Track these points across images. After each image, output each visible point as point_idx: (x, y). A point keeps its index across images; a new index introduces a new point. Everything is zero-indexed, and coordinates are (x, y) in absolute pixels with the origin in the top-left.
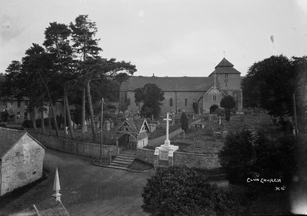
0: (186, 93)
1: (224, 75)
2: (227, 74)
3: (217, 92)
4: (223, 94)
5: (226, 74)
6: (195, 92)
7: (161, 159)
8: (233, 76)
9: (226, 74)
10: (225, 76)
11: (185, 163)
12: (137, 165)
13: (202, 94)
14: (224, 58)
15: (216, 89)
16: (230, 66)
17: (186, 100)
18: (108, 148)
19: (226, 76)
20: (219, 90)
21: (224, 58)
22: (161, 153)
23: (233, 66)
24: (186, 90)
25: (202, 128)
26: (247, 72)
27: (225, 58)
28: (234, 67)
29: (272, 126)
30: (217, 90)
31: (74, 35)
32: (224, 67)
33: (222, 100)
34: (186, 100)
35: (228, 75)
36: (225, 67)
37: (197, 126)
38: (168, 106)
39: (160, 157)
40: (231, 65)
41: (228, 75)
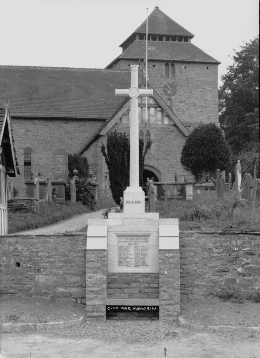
2: (173, 63)
3: (152, 119)
5: (170, 64)
8: (196, 71)
9: (167, 63)
12: (207, 188)
13: (100, 124)
14: (157, 8)
15: (149, 108)
16: (180, 38)
17: (132, 255)
18: (250, 230)
19: (167, 73)
20: (162, 111)
21: (157, 8)
26: (225, 75)
27: (160, 9)
28: (193, 41)
29: (200, 284)
30: (152, 110)
31: (185, 317)
33: (185, 149)
34: (132, 255)
35: (177, 66)
36: (161, 43)
38: (76, 202)
39: (114, 257)
40: (182, 34)
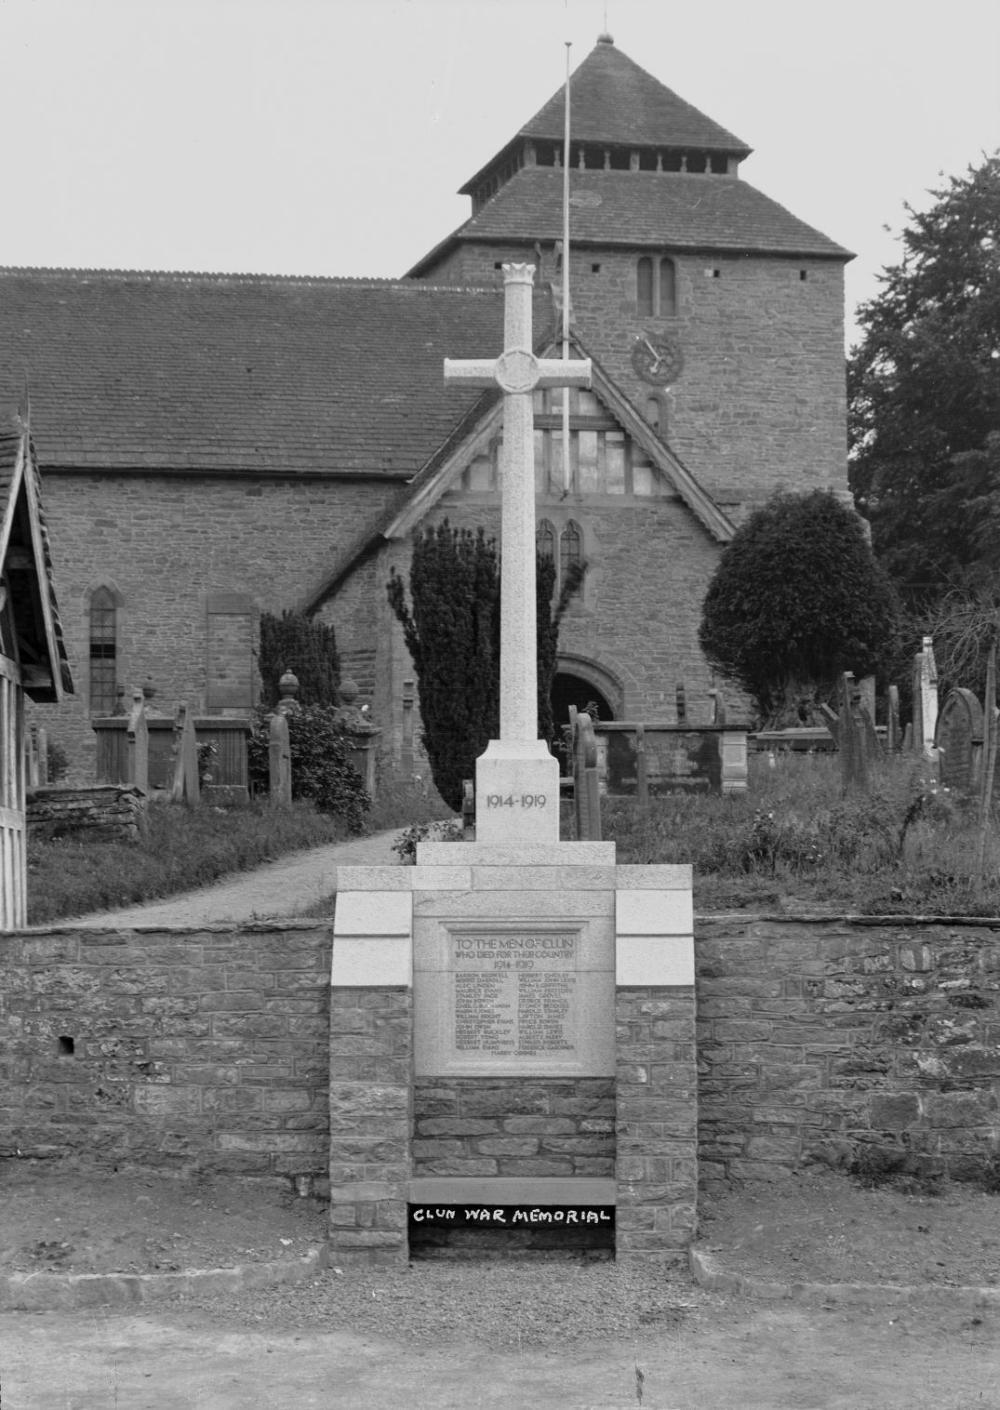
0: (106, 497)
1: (630, 271)
2: (669, 254)
3: (590, 475)
4: (678, 501)
6: (234, 494)
7: (450, 1061)
9: (645, 254)
10: (633, 296)
11: (926, 1081)
14: (606, 41)
15: (574, 432)
16: (697, 159)
19: (646, 293)
20: (628, 443)
21: (606, 41)
22: (442, 950)
23: (742, 153)
24: (105, 460)
25: (716, 781)
27: (617, 45)
28: (746, 171)
30: (589, 439)
32: (620, 156)
35: (684, 268)
36: (624, 176)
37: (652, 766)
39: (439, 1016)
40: (702, 142)
41: (684, 268)
